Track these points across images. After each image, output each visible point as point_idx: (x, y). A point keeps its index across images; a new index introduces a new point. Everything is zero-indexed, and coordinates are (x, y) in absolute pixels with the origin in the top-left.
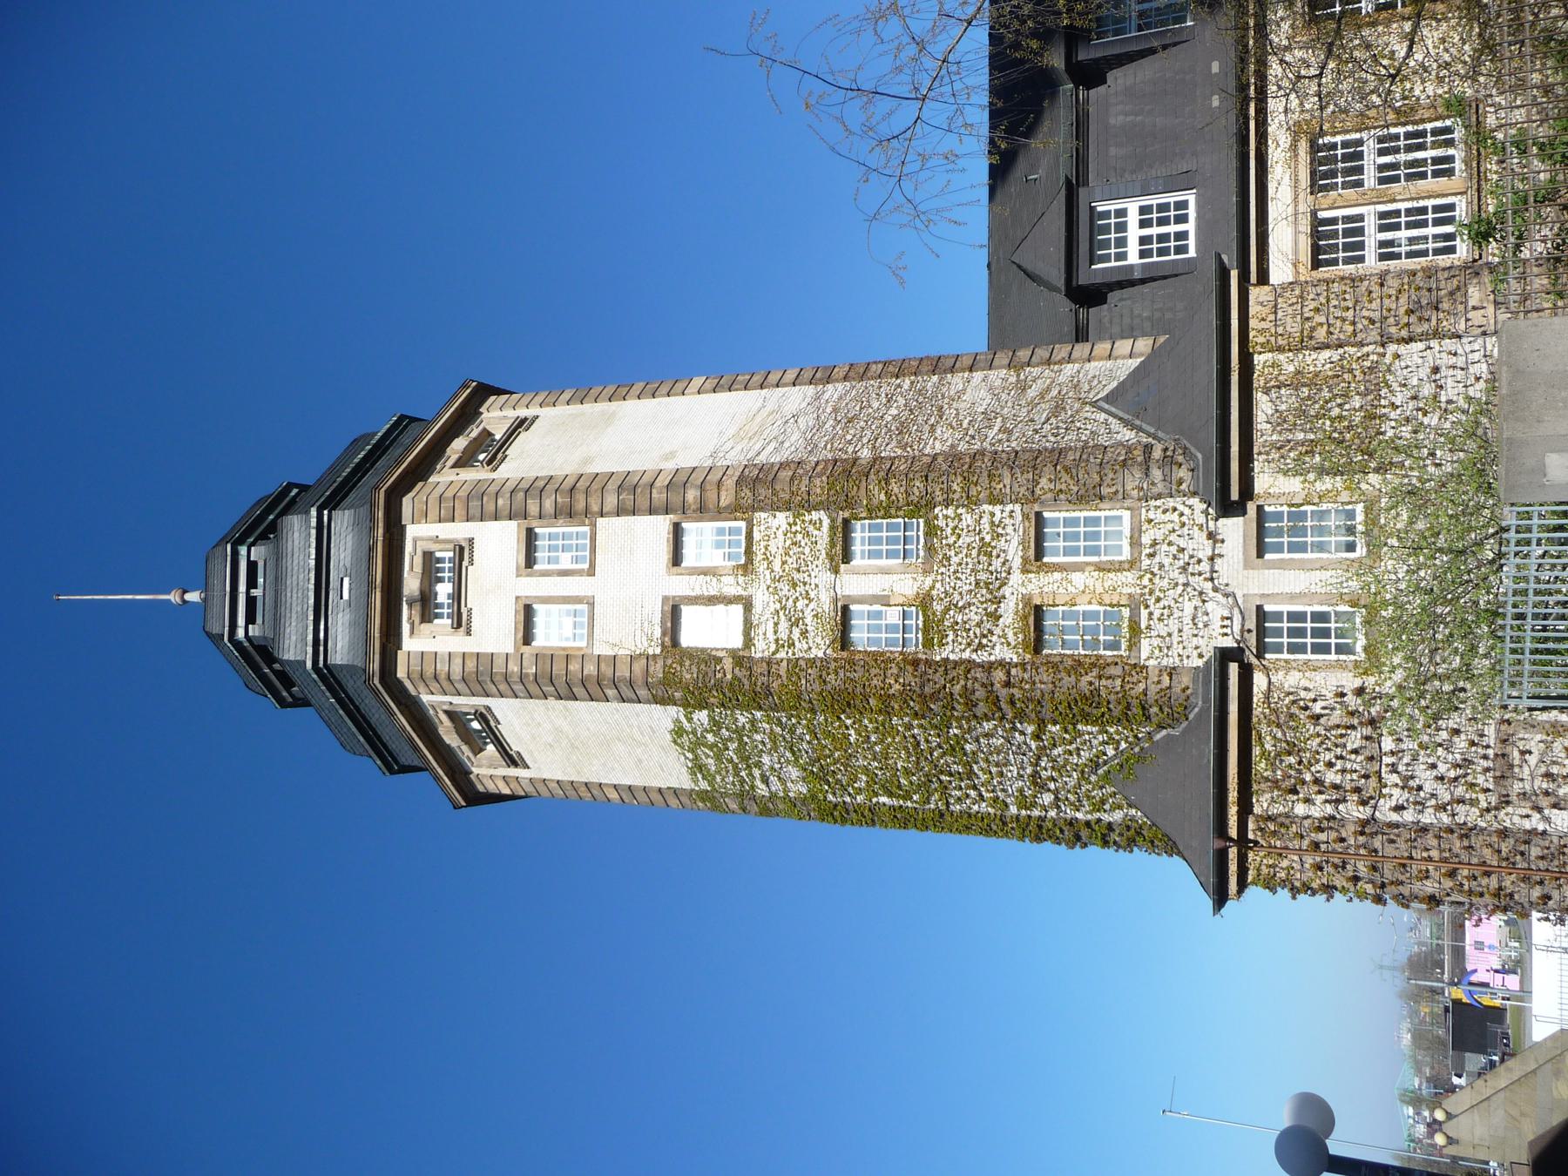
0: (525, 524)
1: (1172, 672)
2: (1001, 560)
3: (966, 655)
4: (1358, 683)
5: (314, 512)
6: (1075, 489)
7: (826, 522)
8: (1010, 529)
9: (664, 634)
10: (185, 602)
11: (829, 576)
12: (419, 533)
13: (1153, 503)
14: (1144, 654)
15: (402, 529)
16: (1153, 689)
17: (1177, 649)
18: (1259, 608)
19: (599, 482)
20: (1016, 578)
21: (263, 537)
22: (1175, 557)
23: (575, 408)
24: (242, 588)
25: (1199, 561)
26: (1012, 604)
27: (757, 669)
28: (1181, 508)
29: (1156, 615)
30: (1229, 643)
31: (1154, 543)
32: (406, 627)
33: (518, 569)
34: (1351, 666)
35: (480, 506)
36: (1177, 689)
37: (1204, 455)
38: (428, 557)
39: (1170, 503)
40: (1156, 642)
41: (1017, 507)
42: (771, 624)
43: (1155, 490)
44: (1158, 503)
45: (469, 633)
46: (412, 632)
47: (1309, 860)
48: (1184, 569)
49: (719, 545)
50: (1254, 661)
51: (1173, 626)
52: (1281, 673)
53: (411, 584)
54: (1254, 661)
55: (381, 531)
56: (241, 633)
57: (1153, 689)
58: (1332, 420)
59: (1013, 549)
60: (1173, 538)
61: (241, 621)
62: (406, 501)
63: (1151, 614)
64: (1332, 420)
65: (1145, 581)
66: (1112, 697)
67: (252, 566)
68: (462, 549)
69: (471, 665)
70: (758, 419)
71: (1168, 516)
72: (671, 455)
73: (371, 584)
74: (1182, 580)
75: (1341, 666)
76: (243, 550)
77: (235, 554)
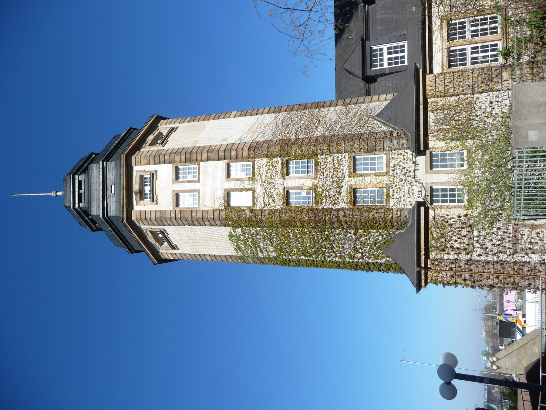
0: (175, 165)
1: (401, 210)
2: (341, 173)
3: (330, 206)
4: (465, 212)
5: (101, 163)
6: (367, 147)
7: (280, 161)
8: (344, 162)
9: (225, 202)
10: (57, 195)
11: (282, 180)
12: (138, 169)
13: (394, 152)
15: (132, 168)
16: (395, 217)
18: (431, 187)
20: (347, 179)
21: (84, 172)
22: (402, 170)
23: (191, 124)
24: (77, 190)
25: (410, 172)
26: (345, 188)
28: (403, 153)
29: (396, 190)
30: (421, 200)
31: (394, 166)
32: (135, 202)
34: (463, 207)
35: (159, 159)
36: (403, 216)
37: (411, 135)
38: (141, 177)
39: (400, 151)
40: (395, 200)
41: (347, 154)
43: (394, 147)
44: (396, 152)
45: (157, 204)
46: (137, 204)
48: (405, 174)
50: (429, 206)
51: (402, 195)
52: (439, 210)
53: (136, 187)
54: (429, 206)
55: (124, 169)
56: (77, 206)
57: (395, 217)
59: (345, 169)
60: (401, 164)
61: (77, 201)
62: (133, 158)
63: (394, 190)
64: (456, 121)
65: (392, 179)
66: (381, 220)
67: (80, 182)
68: (153, 174)
69: (158, 215)
70: (256, 126)
71: (399, 156)
72: (226, 139)
73: (122, 188)
75: (459, 207)
76: (76, 177)
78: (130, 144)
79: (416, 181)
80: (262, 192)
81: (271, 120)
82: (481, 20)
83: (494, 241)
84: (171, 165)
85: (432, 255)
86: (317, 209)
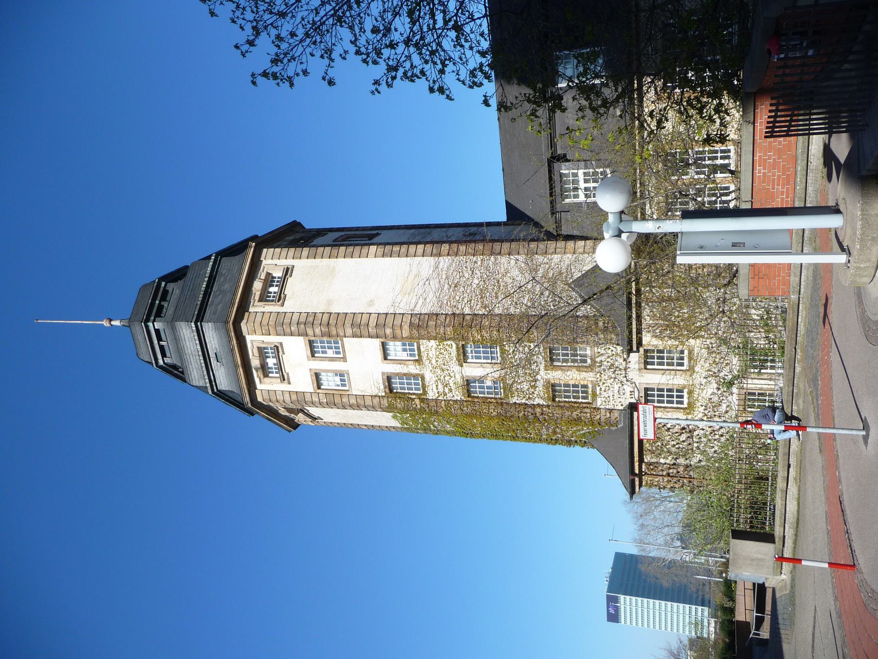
1: (611, 411)
3: (523, 401)
5: (193, 325)
7: (454, 346)
9: (385, 388)
11: (459, 368)
12: (253, 340)
14: (599, 404)
15: (244, 338)
17: (612, 402)
19: (341, 317)
20: (542, 372)
23: (311, 261)
24: (155, 341)
27: (432, 404)
29: (603, 389)
30: (633, 401)
32: (257, 380)
37: (622, 329)
38: (260, 349)
42: (434, 386)
45: (289, 383)
46: (261, 382)
47: (666, 479)
49: (405, 350)
53: (255, 362)
55: (235, 342)
56: (161, 362)
58: (675, 317)
62: (243, 325)
64: (675, 317)
67: (157, 332)
68: (277, 347)
69: (294, 397)
70: (410, 280)
72: (371, 303)
74: (613, 376)
76: (150, 324)
77: (147, 327)
78: (233, 304)
79: (627, 381)
80: (434, 379)
81: (431, 272)
82: (716, 158)
83: (716, 448)
84: (301, 338)
85: (647, 458)
86: (507, 404)
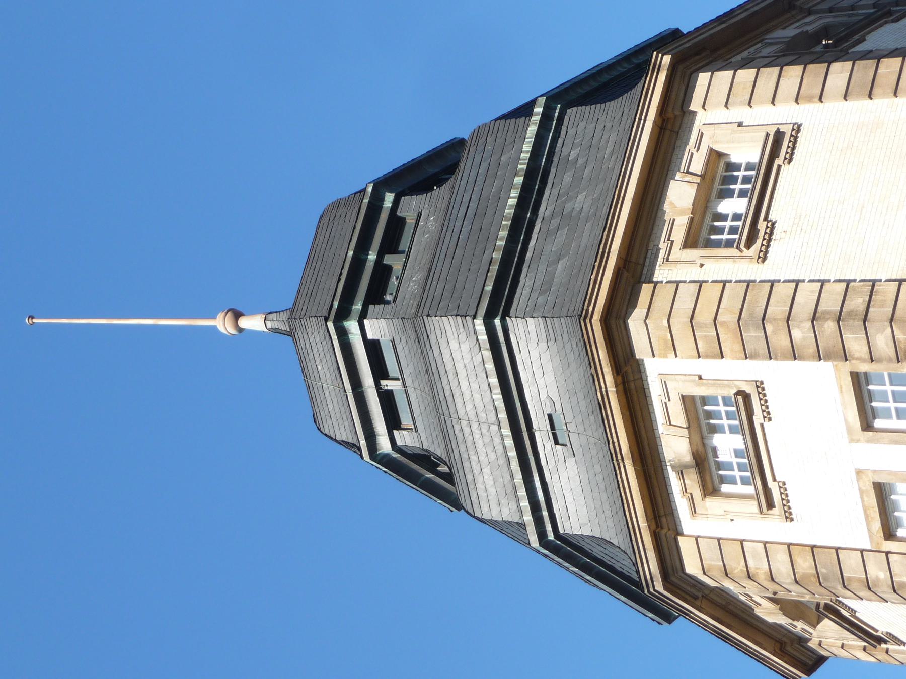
0: (847, 367)
10: (240, 330)
12: (669, 375)
15: (638, 367)
21: (376, 296)
23: (859, 106)
24: (368, 380)
32: (681, 505)
33: (849, 430)
35: (759, 323)
46: (694, 511)
53: (675, 446)
55: (609, 378)
61: (380, 426)
62: (635, 323)
67: (373, 348)
68: (746, 397)
73: (614, 456)
76: (352, 326)
77: (343, 334)
84: (826, 367)
